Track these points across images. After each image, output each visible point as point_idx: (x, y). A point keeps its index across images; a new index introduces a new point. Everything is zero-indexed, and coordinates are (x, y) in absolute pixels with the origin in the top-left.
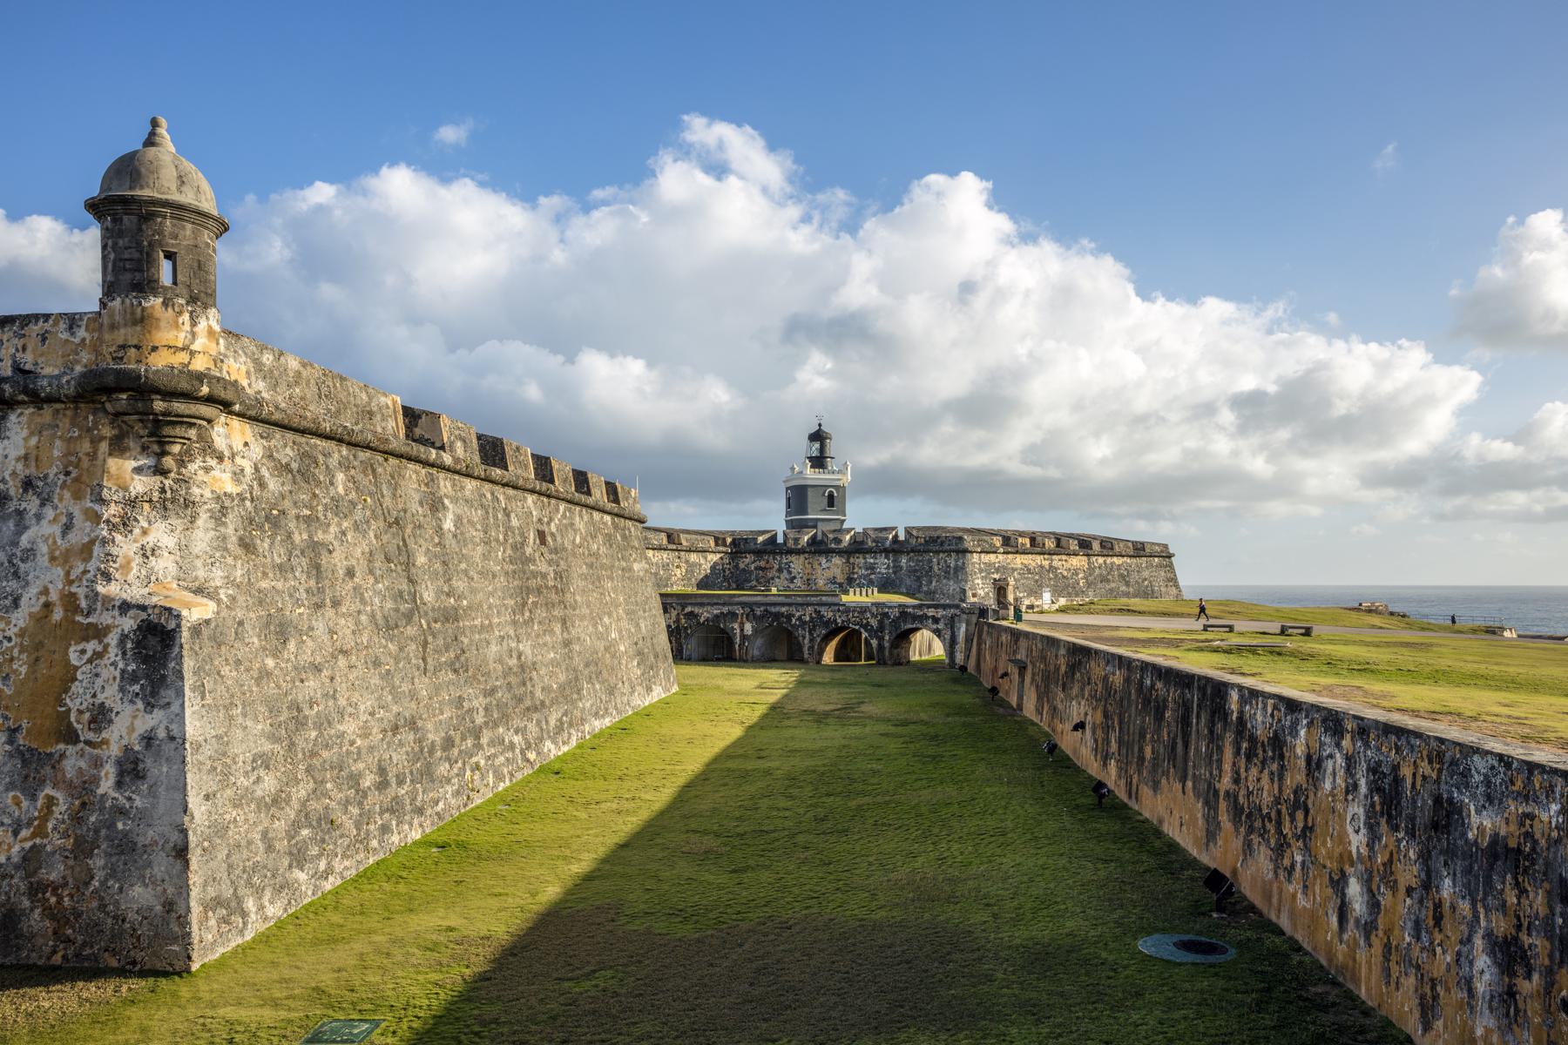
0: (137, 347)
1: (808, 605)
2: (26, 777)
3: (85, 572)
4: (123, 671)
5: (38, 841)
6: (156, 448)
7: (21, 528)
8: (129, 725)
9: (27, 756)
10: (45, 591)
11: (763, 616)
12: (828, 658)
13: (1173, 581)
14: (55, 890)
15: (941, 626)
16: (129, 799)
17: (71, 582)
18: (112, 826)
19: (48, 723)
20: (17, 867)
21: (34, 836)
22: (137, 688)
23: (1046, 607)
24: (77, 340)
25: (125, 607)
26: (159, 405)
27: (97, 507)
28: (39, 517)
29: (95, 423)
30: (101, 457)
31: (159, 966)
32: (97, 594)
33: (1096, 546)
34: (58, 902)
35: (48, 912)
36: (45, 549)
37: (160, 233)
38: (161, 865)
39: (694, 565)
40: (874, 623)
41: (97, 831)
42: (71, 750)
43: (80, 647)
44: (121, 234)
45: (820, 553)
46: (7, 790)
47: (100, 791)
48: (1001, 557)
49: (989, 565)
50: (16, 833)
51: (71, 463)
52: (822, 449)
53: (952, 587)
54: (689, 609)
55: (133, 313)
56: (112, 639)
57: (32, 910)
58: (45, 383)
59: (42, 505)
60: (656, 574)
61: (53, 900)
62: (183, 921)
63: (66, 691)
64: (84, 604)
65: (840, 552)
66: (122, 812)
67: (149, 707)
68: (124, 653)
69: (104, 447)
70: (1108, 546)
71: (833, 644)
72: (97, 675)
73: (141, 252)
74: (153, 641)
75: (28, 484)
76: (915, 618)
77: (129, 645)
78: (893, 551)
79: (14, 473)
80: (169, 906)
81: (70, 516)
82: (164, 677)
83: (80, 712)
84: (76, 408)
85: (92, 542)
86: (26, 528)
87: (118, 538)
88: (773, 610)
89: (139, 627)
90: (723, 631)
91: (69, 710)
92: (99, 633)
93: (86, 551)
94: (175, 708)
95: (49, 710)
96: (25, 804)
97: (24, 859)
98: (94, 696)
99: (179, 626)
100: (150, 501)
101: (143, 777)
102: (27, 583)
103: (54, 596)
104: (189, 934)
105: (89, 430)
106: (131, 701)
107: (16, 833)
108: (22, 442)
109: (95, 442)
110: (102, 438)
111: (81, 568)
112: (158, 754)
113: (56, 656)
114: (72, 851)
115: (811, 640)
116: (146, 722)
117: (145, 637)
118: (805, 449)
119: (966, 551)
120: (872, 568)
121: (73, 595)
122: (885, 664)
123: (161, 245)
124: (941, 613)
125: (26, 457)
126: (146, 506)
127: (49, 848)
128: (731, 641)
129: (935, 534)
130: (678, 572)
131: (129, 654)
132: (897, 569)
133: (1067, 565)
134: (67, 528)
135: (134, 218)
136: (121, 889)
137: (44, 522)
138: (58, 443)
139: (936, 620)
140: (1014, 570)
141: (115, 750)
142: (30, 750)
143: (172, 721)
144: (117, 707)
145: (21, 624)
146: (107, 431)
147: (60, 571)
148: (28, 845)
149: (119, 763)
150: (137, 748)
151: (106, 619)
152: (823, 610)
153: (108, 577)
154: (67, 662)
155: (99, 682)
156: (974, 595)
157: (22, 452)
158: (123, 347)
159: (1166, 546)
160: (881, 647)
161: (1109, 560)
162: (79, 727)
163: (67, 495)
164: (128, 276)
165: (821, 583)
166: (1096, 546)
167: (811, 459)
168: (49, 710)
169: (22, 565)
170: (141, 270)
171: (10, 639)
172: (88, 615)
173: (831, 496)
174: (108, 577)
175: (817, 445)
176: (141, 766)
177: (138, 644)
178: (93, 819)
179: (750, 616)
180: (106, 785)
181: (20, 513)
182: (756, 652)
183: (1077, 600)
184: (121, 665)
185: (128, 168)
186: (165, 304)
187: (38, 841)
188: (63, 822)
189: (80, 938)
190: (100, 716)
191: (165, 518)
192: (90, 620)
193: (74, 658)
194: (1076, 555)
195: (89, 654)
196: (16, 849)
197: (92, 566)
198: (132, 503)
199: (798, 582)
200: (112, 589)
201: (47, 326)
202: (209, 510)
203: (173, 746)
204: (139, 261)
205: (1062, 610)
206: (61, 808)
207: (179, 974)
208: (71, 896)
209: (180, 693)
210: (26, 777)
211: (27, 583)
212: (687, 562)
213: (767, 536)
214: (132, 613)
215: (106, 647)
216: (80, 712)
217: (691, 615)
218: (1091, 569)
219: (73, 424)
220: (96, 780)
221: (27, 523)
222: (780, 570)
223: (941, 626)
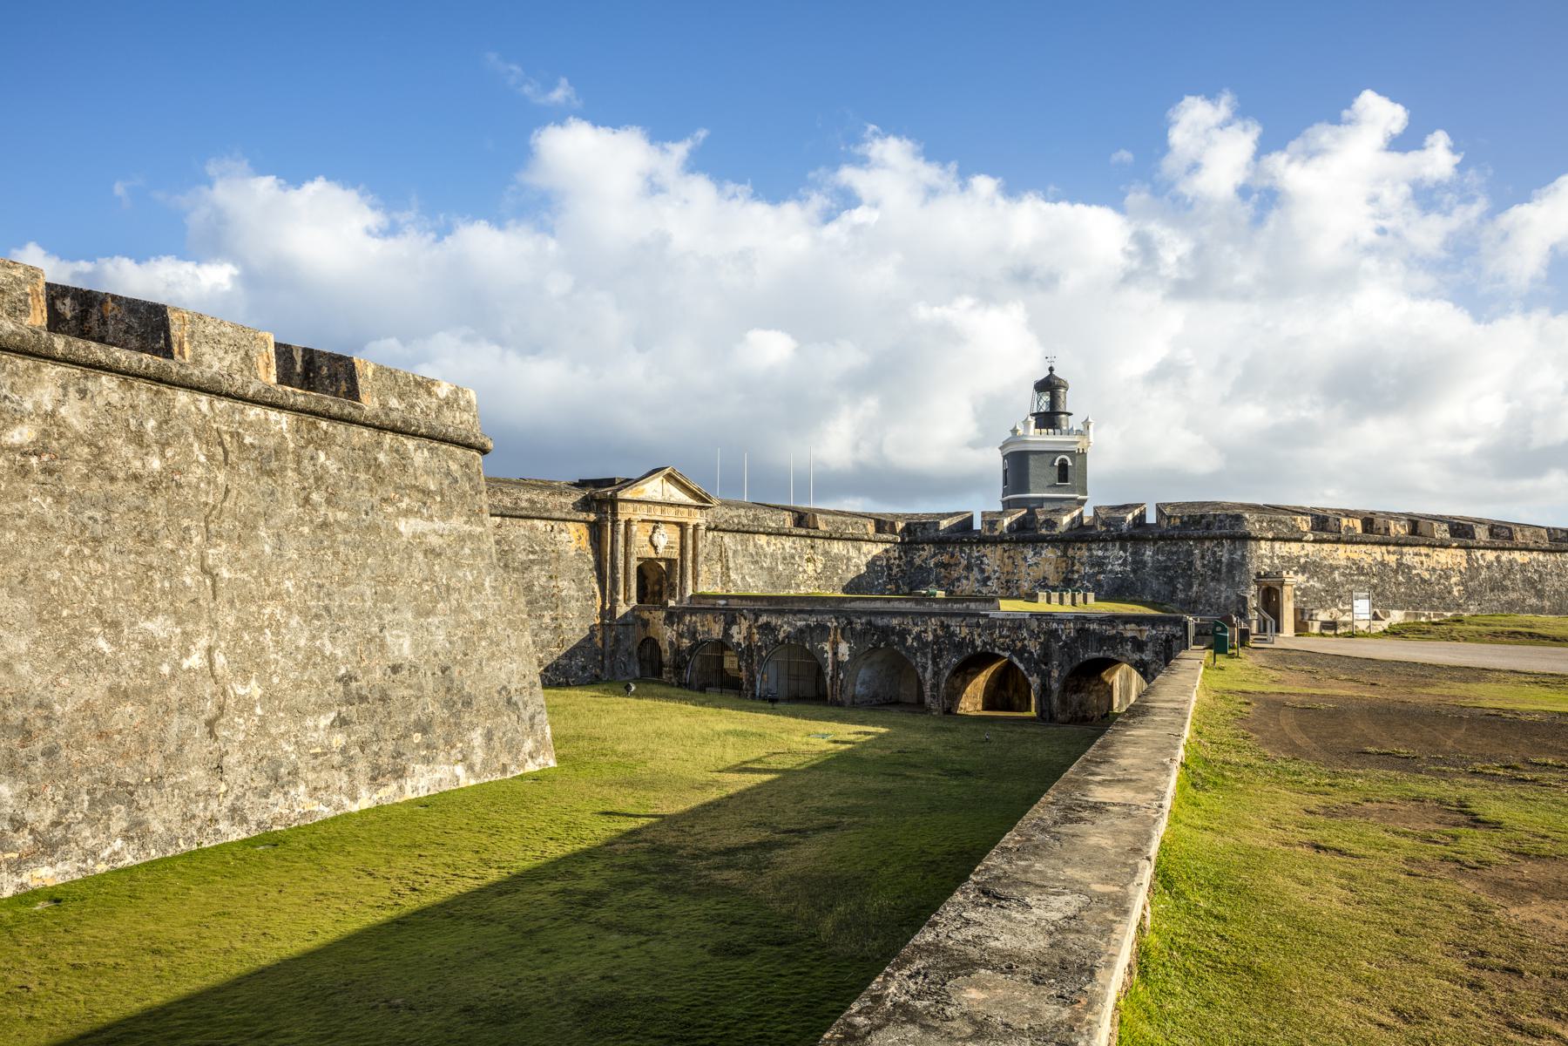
1: (932, 614)
11: (864, 633)
12: (971, 701)
23: (1362, 626)
33: (1482, 534)
39: (838, 558)
40: (1034, 647)
45: (1025, 542)
48: (1309, 548)
52: (1053, 403)
54: (764, 619)
60: (770, 570)
65: (1054, 541)
70: (1502, 535)
71: (981, 680)
76: (1102, 640)
88: (880, 622)
90: (809, 654)
115: (936, 674)
118: (1029, 402)
119: (1247, 538)
120: (1100, 564)
122: (1052, 719)
124: (1147, 632)
128: (819, 670)
130: (810, 567)
132: (1138, 564)
133: (1432, 564)
139: (1139, 645)
140: (1333, 568)
152: (953, 623)
161: (1505, 556)
166: (1482, 534)
173: (1063, 467)
175: (1046, 398)
179: (848, 632)
182: (860, 690)
183: (1426, 616)
205: (1395, 632)
212: (826, 553)
213: (955, 520)
217: (767, 628)
218: (1474, 570)
222: (969, 568)
223: (1147, 656)
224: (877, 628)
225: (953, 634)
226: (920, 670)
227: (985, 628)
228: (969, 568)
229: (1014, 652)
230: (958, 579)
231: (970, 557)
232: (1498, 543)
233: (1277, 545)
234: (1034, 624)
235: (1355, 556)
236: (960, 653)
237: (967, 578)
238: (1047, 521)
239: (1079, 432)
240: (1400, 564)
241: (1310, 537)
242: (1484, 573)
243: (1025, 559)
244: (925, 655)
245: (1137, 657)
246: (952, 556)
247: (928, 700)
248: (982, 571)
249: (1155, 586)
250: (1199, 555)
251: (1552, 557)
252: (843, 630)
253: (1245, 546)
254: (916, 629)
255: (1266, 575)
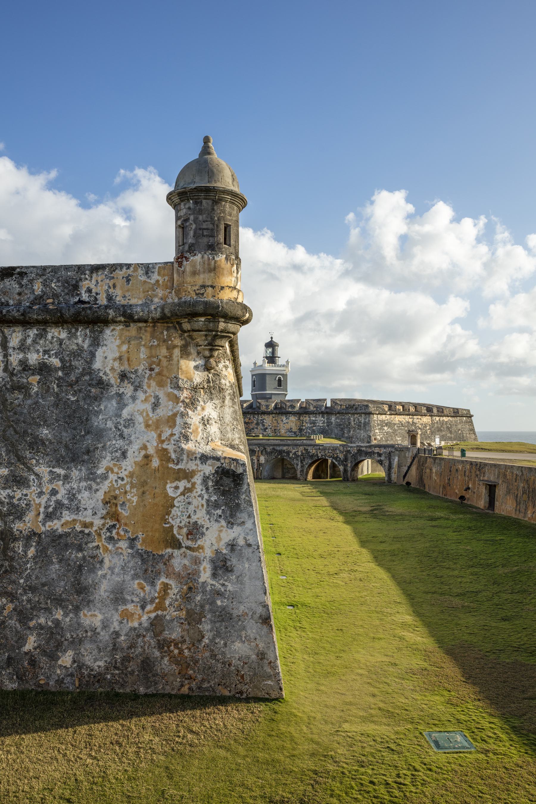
0: (213, 287)
2: (146, 570)
3: (172, 435)
4: (208, 501)
5: (160, 613)
6: (207, 353)
7: (122, 405)
8: (216, 536)
9: (145, 556)
10: (145, 447)
11: (271, 453)
12: (310, 477)
13: (472, 430)
14: (176, 645)
15: (382, 458)
16: (223, 585)
17: (163, 442)
18: (213, 603)
19: (157, 535)
20: (147, 630)
21: (156, 609)
22: (219, 512)
24: (153, 281)
25: (204, 458)
26: (222, 325)
27: (176, 392)
28: (134, 398)
29: (169, 337)
30: (175, 358)
31: (260, 695)
32: (182, 449)
33: (435, 410)
34: (180, 653)
35: (174, 660)
36: (141, 419)
37: (224, 212)
38: (253, 628)
40: (341, 456)
41: (202, 606)
42: (176, 552)
43: (174, 485)
44: (200, 212)
45: (282, 414)
46: (133, 579)
47: (201, 580)
48: (388, 417)
49: (382, 421)
50: (143, 608)
51: (154, 363)
52: (273, 352)
53: (362, 434)
55: (209, 264)
56: (198, 479)
57: (162, 658)
58: (139, 309)
59: (136, 390)
61: (176, 651)
62: (273, 665)
63: (169, 513)
64: (173, 456)
65: (294, 414)
66: (219, 593)
67: (231, 524)
68: (207, 489)
69: (177, 352)
70: (441, 411)
72: (189, 503)
73: (213, 224)
74: (227, 481)
75: (123, 376)
77: (210, 484)
78: (327, 413)
79: (112, 369)
80: (262, 656)
81: (157, 398)
82: (238, 505)
83: (180, 528)
84: (154, 327)
85: (175, 415)
86: (125, 405)
87: (190, 412)
88: (278, 448)
89: (217, 472)
91: (172, 526)
92: (188, 475)
93: (171, 421)
94: (249, 525)
95: (157, 526)
96: (148, 588)
97: (152, 624)
98: (189, 517)
99: (245, 471)
100: (203, 388)
101: (232, 571)
102: (131, 442)
103: (151, 451)
104: (279, 673)
105: (164, 341)
106: (216, 521)
107: (143, 608)
108: (116, 348)
109: (170, 349)
110: (175, 347)
111: (169, 432)
112: (240, 556)
113: (157, 490)
114: (186, 620)
115: (302, 466)
116: (228, 535)
117: (221, 478)
119: (370, 413)
121: (166, 450)
122: (348, 480)
123: (224, 220)
124: (383, 450)
125: (120, 358)
126: (202, 390)
127: (168, 617)
129: (352, 403)
131: (211, 490)
132: (329, 423)
133: (421, 422)
134: (156, 405)
135: (210, 202)
136: (225, 645)
137: (138, 402)
138: (142, 349)
139: (380, 455)
140: (395, 424)
141: (208, 553)
142: (147, 552)
143: (248, 534)
144: (207, 524)
145: (130, 469)
146: (178, 342)
147: (153, 435)
148: (153, 615)
149: (212, 561)
150: (224, 551)
151: (192, 466)
152: (309, 449)
153: (187, 438)
154: (166, 495)
155: (191, 508)
156: (375, 439)
157: (117, 355)
158: (203, 286)
159: (469, 411)
160: (345, 471)
161: (442, 419)
162: (180, 537)
163: (153, 383)
164: (205, 240)
165: (283, 431)
167: (267, 357)
168: (157, 526)
169: (125, 430)
170: (213, 236)
171: (123, 479)
172: (177, 464)
173: (280, 380)
174: (187, 438)
176: (229, 564)
177: (217, 483)
178: (198, 598)
180: (205, 575)
181: (120, 396)
184: (206, 497)
185: (203, 165)
186: (227, 259)
187: (160, 613)
188: (176, 600)
189: (200, 677)
190: (195, 531)
191: (212, 399)
192: (179, 467)
193: (170, 492)
194: (425, 416)
195: (181, 489)
196: (145, 618)
197: (177, 430)
198: (195, 389)
199: (269, 431)
200: (189, 446)
201: (130, 272)
202: (229, 394)
203: (250, 550)
204: (212, 230)
206: (175, 589)
207: (277, 699)
208: (190, 649)
209: (251, 515)
210: (146, 570)
211: (131, 442)
213: (248, 404)
214: (210, 462)
215: (194, 484)
216: (180, 528)
219: (153, 337)
220: (197, 573)
221: (126, 402)
222: (257, 424)
223: (382, 458)
224: (277, 450)
225: (309, 452)
226: (295, 466)
227: (322, 450)
228: (257, 424)
229: (333, 458)
230: (253, 429)
231: (258, 420)
232: (440, 414)
233: (379, 416)
234: (341, 448)
235: (400, 420)
236: (312, 459)
237: (257, 428)
238: (291, 406)
239: (283, 366)
240: (413, 422)
241: (389, 413)
242: (436, 425)
243: (282, 421)
244: (298, 460)
245: (379, 458)
246: (250, 419)
247: (299, 476)
248: (264, 425)
249: (336, 431)
250: (353, 420)
251: (454, 419)
252: (262, 452)
253: (369, 417)
254: (294, 451)
255: (412, 431)
